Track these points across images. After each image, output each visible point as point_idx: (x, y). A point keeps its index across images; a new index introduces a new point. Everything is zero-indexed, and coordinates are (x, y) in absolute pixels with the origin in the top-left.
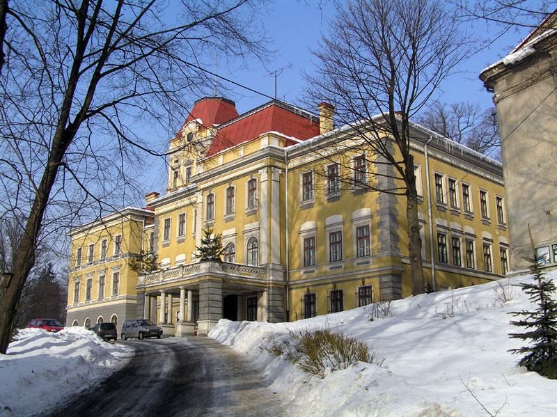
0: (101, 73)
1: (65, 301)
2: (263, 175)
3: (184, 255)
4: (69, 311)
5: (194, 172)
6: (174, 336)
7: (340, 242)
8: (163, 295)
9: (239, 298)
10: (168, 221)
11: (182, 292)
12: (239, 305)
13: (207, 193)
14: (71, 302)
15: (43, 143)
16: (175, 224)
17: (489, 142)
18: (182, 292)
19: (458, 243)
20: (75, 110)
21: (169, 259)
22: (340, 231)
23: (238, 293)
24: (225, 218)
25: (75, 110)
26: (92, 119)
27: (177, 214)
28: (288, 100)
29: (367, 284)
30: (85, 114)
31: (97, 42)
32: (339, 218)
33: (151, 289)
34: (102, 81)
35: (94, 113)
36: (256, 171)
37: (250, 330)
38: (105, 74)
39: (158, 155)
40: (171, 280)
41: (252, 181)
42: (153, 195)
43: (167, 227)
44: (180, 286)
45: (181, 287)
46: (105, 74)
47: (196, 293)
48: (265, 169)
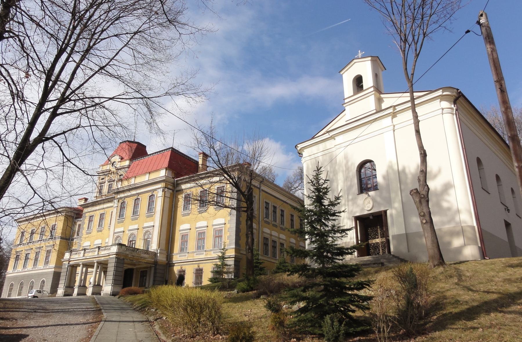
0: (58, 113)
1: (6, 269)
2: (160, 193)
3: (101, 240)
4: (7, 276)
5: (115, 187)
6: (85, 294)
7: (204, 239)
8: (81, 266)
9: (135, 271)
10: (91, 217)
11: (96, 264)
12: (134, 275)
13: (121, 201)
14: (10, 269)
15: (6, 154)
16: (96, 219)
17: (297, 187)
18: (96, 264)
19: (275, 244)
20: (34, 135)
21: (90, 242)
22: (205, 232)
23: (134, 267)
24: (147, 215)
25: (34, 135)
26: (47, 144)
27: (98, 213)
28: (183, 150)
29: (201, 267)
30: (42, 138)
31: (55, 95)
32: (204, 223)
33: (73, 262)
34: (57, 119)
35: (47, 139)
36: (156, 190)
37: (472, 284)
38: (62, 114)
39: (89, 175)
40: (92, 256)
41: (151, 197)
42: (84, 200)
43: (90, 221)
44: (80, 262)
45: (95, 261)
46: (62, 114)
47: (105, 266)
48: (162, 189)
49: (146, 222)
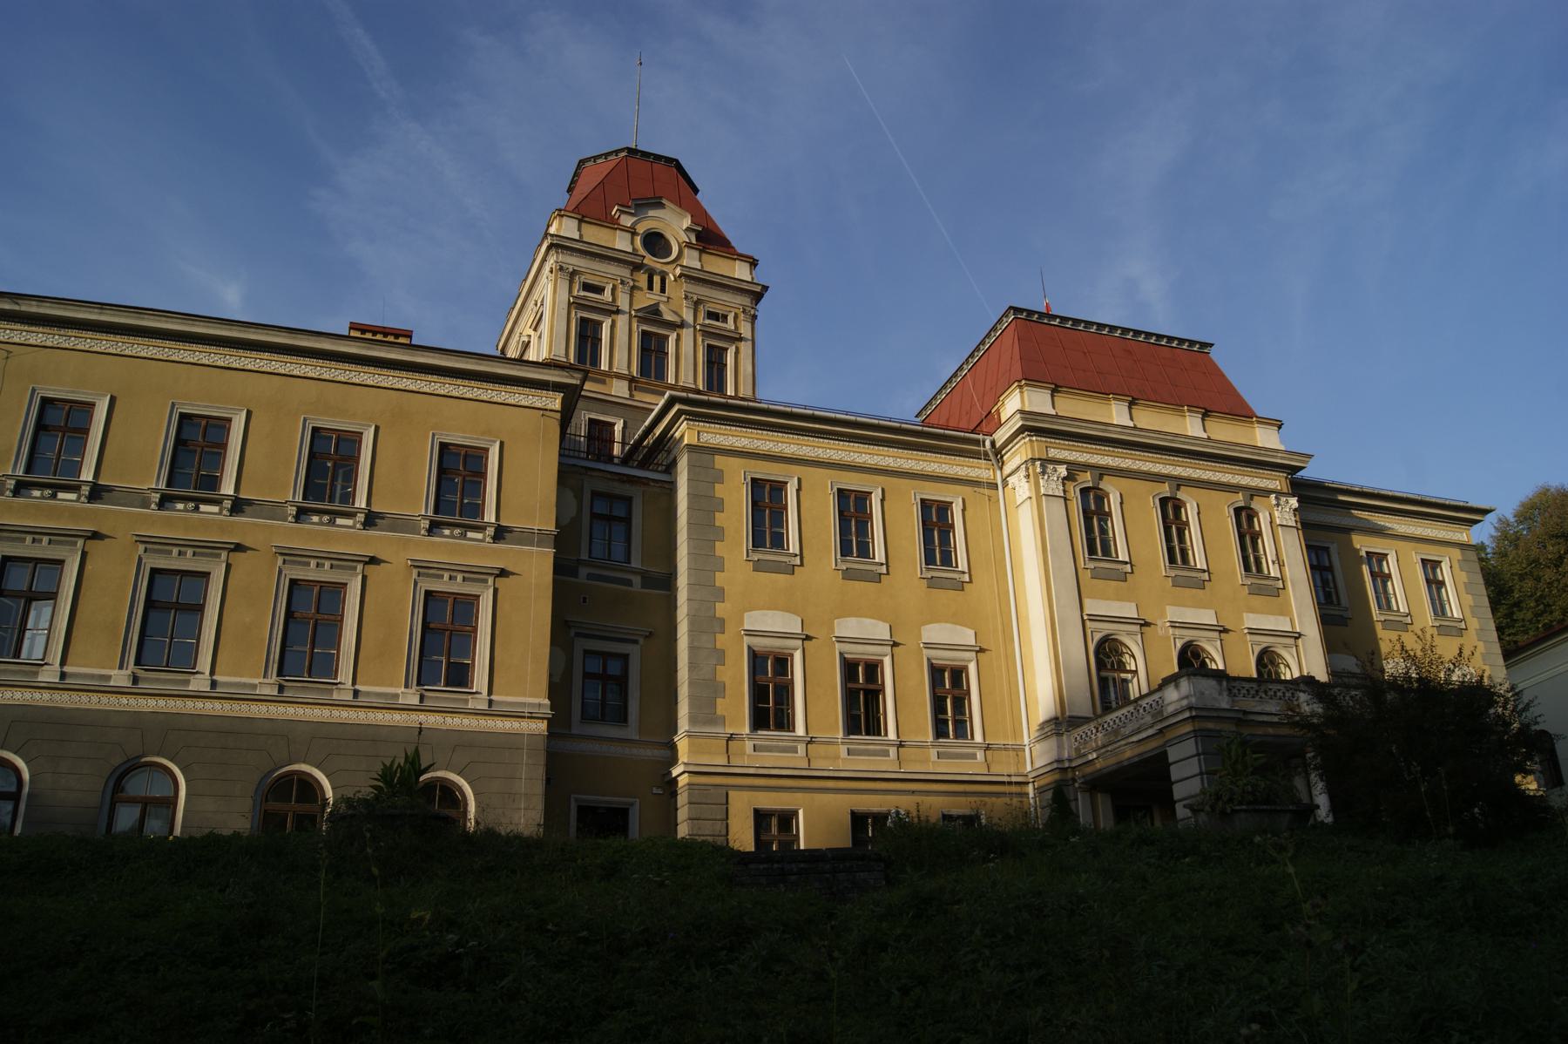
49: (1252, 610)
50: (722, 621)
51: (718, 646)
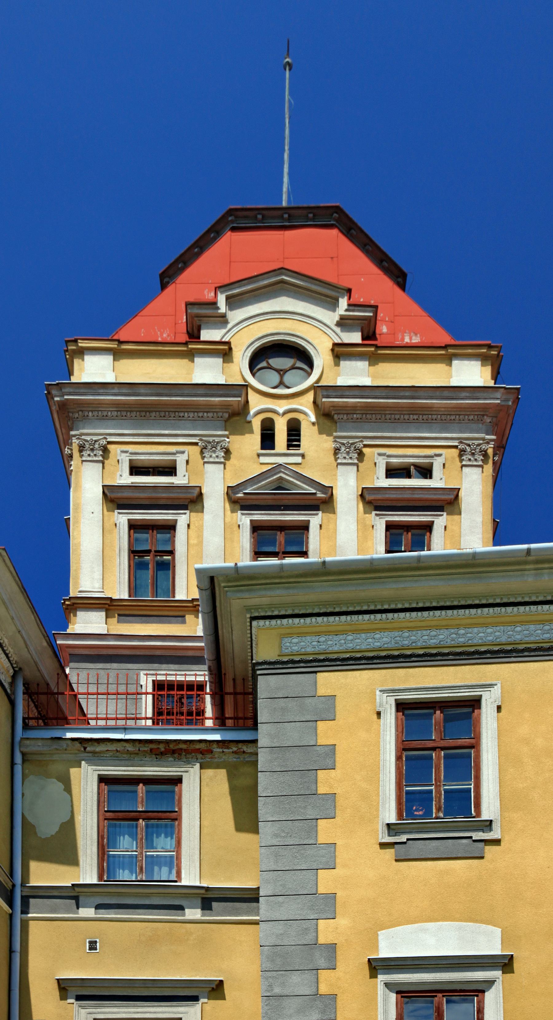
50: (332, 948)
51: (323, 989)
